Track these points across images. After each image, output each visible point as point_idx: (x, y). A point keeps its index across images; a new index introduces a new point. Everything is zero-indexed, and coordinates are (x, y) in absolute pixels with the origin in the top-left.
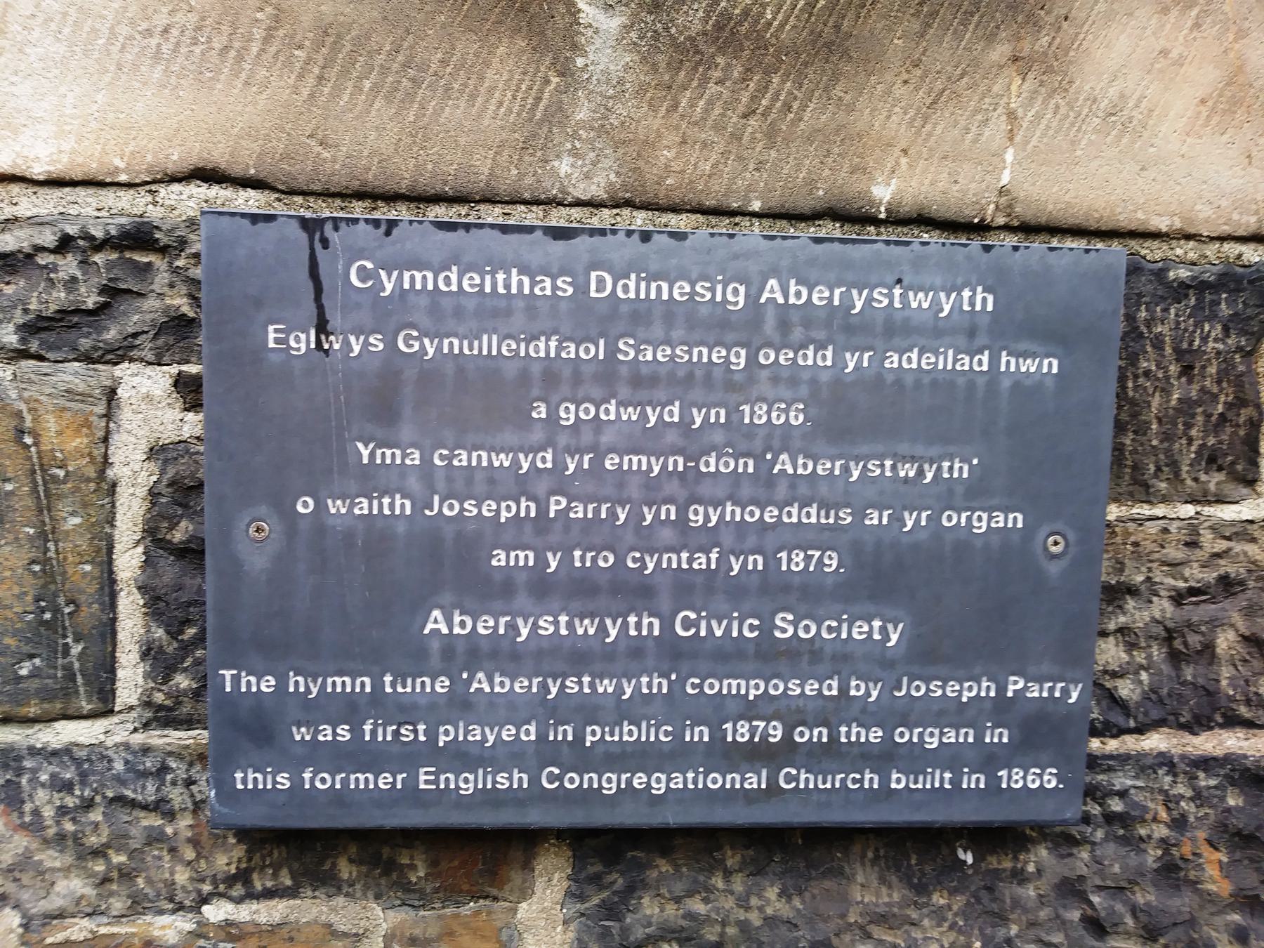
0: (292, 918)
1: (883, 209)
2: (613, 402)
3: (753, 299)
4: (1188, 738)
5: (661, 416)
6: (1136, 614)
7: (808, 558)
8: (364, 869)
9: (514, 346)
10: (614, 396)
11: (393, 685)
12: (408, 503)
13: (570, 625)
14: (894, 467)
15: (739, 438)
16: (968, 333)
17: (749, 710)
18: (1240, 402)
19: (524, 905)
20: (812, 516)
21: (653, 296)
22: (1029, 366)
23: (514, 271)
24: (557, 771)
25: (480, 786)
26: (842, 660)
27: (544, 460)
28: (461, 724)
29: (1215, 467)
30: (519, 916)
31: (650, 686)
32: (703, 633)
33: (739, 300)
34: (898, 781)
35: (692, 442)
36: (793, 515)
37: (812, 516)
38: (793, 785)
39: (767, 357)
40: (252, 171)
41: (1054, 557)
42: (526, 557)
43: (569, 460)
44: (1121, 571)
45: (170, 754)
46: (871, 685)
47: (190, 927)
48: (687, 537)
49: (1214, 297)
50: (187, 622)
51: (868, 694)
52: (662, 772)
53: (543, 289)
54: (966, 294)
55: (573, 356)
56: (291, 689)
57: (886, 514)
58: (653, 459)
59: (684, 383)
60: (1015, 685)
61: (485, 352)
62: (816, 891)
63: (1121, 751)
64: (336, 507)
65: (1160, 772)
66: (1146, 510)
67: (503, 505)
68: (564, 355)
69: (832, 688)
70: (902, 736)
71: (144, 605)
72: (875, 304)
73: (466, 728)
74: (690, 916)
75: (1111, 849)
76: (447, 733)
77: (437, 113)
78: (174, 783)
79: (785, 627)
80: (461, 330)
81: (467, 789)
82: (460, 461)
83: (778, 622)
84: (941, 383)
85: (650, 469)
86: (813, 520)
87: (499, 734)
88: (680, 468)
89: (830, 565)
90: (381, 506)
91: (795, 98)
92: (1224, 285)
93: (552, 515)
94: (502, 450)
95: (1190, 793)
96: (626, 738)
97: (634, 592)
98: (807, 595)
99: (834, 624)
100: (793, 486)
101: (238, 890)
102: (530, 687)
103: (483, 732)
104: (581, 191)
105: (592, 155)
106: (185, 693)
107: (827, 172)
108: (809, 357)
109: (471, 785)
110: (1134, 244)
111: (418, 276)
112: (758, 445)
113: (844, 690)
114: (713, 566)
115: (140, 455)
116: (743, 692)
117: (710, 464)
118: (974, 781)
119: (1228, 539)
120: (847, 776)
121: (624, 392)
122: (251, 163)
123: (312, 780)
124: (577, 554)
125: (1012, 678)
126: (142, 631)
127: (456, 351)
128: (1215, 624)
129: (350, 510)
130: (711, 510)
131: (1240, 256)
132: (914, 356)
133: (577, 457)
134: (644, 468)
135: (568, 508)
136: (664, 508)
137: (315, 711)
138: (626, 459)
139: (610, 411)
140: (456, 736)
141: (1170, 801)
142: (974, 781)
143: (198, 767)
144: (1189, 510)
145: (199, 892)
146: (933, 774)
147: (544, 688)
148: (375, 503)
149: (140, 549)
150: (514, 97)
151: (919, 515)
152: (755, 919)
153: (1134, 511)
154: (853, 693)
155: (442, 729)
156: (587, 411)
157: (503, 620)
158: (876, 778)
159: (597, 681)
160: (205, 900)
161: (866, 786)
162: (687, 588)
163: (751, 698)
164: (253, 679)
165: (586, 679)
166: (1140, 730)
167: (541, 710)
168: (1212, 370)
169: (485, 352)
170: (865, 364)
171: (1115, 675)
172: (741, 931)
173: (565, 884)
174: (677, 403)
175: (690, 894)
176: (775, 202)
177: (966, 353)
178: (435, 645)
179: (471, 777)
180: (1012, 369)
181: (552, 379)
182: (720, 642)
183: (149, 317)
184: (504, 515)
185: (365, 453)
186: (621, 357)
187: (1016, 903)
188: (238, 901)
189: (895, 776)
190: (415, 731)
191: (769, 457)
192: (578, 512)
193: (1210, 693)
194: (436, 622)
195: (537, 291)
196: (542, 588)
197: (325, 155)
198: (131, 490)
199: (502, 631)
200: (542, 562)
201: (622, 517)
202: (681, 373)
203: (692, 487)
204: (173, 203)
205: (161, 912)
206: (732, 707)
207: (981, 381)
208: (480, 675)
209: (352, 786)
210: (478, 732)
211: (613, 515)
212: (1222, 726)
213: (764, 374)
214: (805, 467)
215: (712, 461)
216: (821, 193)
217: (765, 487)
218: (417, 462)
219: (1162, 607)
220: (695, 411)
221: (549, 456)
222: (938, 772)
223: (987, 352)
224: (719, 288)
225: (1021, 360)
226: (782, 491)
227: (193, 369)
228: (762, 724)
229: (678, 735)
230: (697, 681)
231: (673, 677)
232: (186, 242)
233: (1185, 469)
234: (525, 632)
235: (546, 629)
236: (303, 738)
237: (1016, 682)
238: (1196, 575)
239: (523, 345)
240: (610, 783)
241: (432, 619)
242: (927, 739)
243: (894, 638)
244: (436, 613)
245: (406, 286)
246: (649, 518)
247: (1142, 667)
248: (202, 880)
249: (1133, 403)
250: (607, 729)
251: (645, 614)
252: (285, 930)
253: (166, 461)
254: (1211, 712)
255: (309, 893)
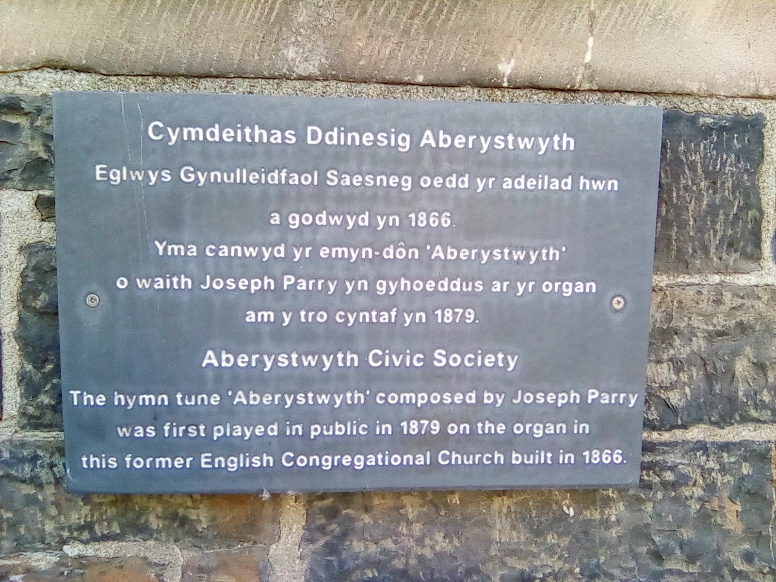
0: (121, 554)
1: (505, 80)
2: (324, 212)
3: (415, 144)
4: (717, 430)
5: (356, 222)
6: (680, 349)
7: (455, 314)
8: (167, 522)
9: (257, 177)
10: (325, 209)
11: (183, 399)
12: (189, 281)
13: (299, 360)
14: (510, 254)
15: (408, 234)
16: (557, 164)
17: (418, 413)
18: (747, 207)
19: (274, 546)
20: (457, 286)
21: (349, 143)
22: (599, 185)
23: (257, 127)
24: (292, 455)
25: (242, 465)
26: (478, 380)
27: (279, 252)
28: (228, 425)
29: (733, 250)
30: (270, 553)
31: (352, 398)
32: (387, 364)
33: (405, 145)
34: (516, 458)
35: (377, 238)
36: (444, 285)
37: (457, 286)
38: (447, 462)
39: (425, 182)
40: (84, 62)
41: (617, 311)
42: (268, 315)
43: (296, 251)
44: (670, 320)
45: (39, 447)
46: (497, 396)
47: (56, 559)
48: (376, 302)
49: (729, 136)
50: (45, 361)
51: (495, 401)
52: (361, 454)
53: (276, 139)
54: (556, 138)
55: (297, 182)
56: (116, 403)
57: (505, 284)
58: (352, 250)
59: (373, 200)
60: (593, 395)
61: (238, 181)
62: (469, 536)
63: (672, 440)
64: (142, 283)
65: (698, 454)
66: (687, 279)
67: (253, 281)
68: (291, 182)
69: (472, 398)
70: (518, 429)
71: (19, 350)
72: (496, 146)
73: (231, 428)
74: (384, 551)
75: (667, 506)
76: (219, 431)
77: (205, 18)
78: (42, 467)
79: (440, 358)
80: (222, 167)
81: (233, 467)
82: (223, 253)
83: (436, 356)
84: (541, 198)
85: (350, 257)
86: (458, 289)
87: (253, 431)
88: (370, 256)
89: (470, 319)
90: (172, 283)
91: (446, 6)
92: (735, 128)
93: (285, 288)
94: (251, 245)
95: (718, 467)
96: (337, 433)
97: (344, 339)
98: (455, 338)
99: (473, 357)
100: (444, 267)
101: (86, 535)
102: (273, 400)
103: (243, 431)
104: (302, 69)
105: (309, 46)
106: (47, 407)
107: (468, 55)
108: (452, 182)
109: (235, 465)
110: (676, 100)
111: (193, 131)
112: (421, 240)
113: (480, 399)
114: (393, 321)
115: (14, 251)
116: (414, 402)
117: (389, 253)
118: (568, 458)
119: (743, 298)
120: (483, 456)
121: (332, 206)
122: (83, 57)
123: (131, 462)
124: (303, 313)
125: (591, 391)
126: (19, 367)
127: (219, 180)
128: (735, 353)
129: (152, 285)
130: (391, 283)
131: (745, 109)
132: (522, 180)
133: (301, 249)
134: (346, 256)
135: (296, 284)
136: (360, 283)
137: (131, 417)
138: (334, 250)
139: (322, 219)
140: (225, 434)
141: (705, 471)
142: (568, 458)
143: (57, 455)
144: (716, 279)
145: (61, 536)
146: (540, 454)
147: (283, 401)
148: (168, 281)
149: (16, 313)
150: (256, 8)
151: (527, 284)
152: (428, 553)
153: (679, 280)
154: (486, 401)
155: (215, 429)
156: (307, 219)
157: (254, 357)
158: (502, 457)
159: (318, 396)
160: (64, 542)
161: (496, 462)
162: (376, 335)
163: (419, 405)
164: (91, 397)
165: (310, 395)
166: (684, 427)
167: (281, 416)
168: (729, 184)
169: (238, 181)
170: (490, 186)
171: (666, 389)
172: (419, 562)
173: (302, 532)
174: (467, 175)
175: (384, 537)
176: (433, 77)
177: (557, 178)
178: (210, 374)
179: (235, 459)
180: (588, 188)
181: (284, 197)
182: (398, 370)
183: (18, 160)
184: (253, 288)
185: (161, 248)
186: (329, 183)
187: (603, 542)
188: (86, 543)
189: (514, 455)
190: (198, 430)
191: (428, 248)
192: (303, 285)
193: (732, 400)
194: (210, 358)
195: (272, 140)
196: (280, 336)
197: (132, 49)
198: (9, 274)
199: (254, 364)
200: (279, 319)
201: (332, 288)
202: (369, 193)
203: (379, 268)
204: (33, 84)
205: (36, 550)
206: (406, 411)
207: (567, 196)
208: (240, 393)
209: (157, 466)
210: (239, 430)
211: (325, 287)
212: (739, 422)
213: (424, 193)
214: (452, 254)
215: (391, 251)
216: (464, 69)
217: (427, 267)
218: (195, 254)
219: (699, 344)
220: (379, 218)
221: (282, 249)
222: (543, 453)
223: (570, 177)
224: (393, 136)
225: (593, 182)
226: (437, 270)
227: (47, 193)
228: (426, 422)
229: (371, 430)
230: (383, 395)
231: (368, 393)
232: (41, 110)
233: (713, 250)
234: (269, 364)
235: (283, 363)
236: (124, 434)
237: (593, 394)
238: (720, 322)
239: (263, 176)
240: (327, 462)
241: (207, 356)
242: (535, 431)
243: (512, 365)
244: (210, 353)
245: (185, 138)
246: (350, 289)
247: (685, 384)
248: (63, 529)
249: (676, 207)
250: (325, 427)
251: (349, 352)
252: (117, 561)
253: (30, 254)
254: (731, 411)
255: (132, 538)
